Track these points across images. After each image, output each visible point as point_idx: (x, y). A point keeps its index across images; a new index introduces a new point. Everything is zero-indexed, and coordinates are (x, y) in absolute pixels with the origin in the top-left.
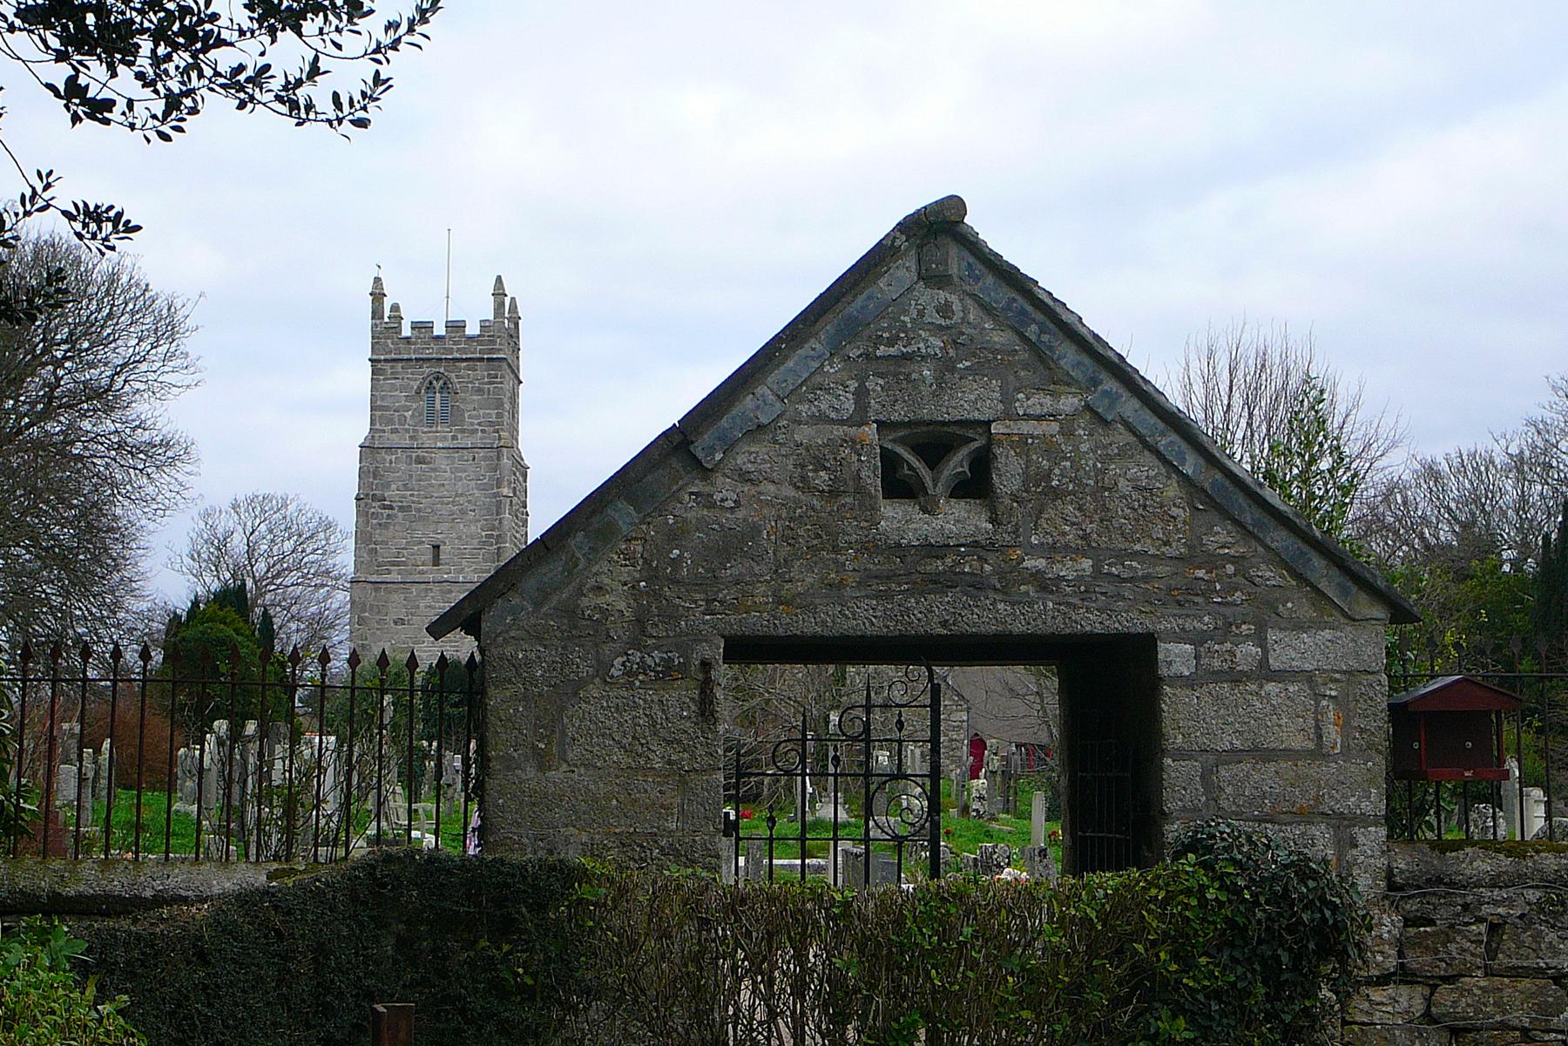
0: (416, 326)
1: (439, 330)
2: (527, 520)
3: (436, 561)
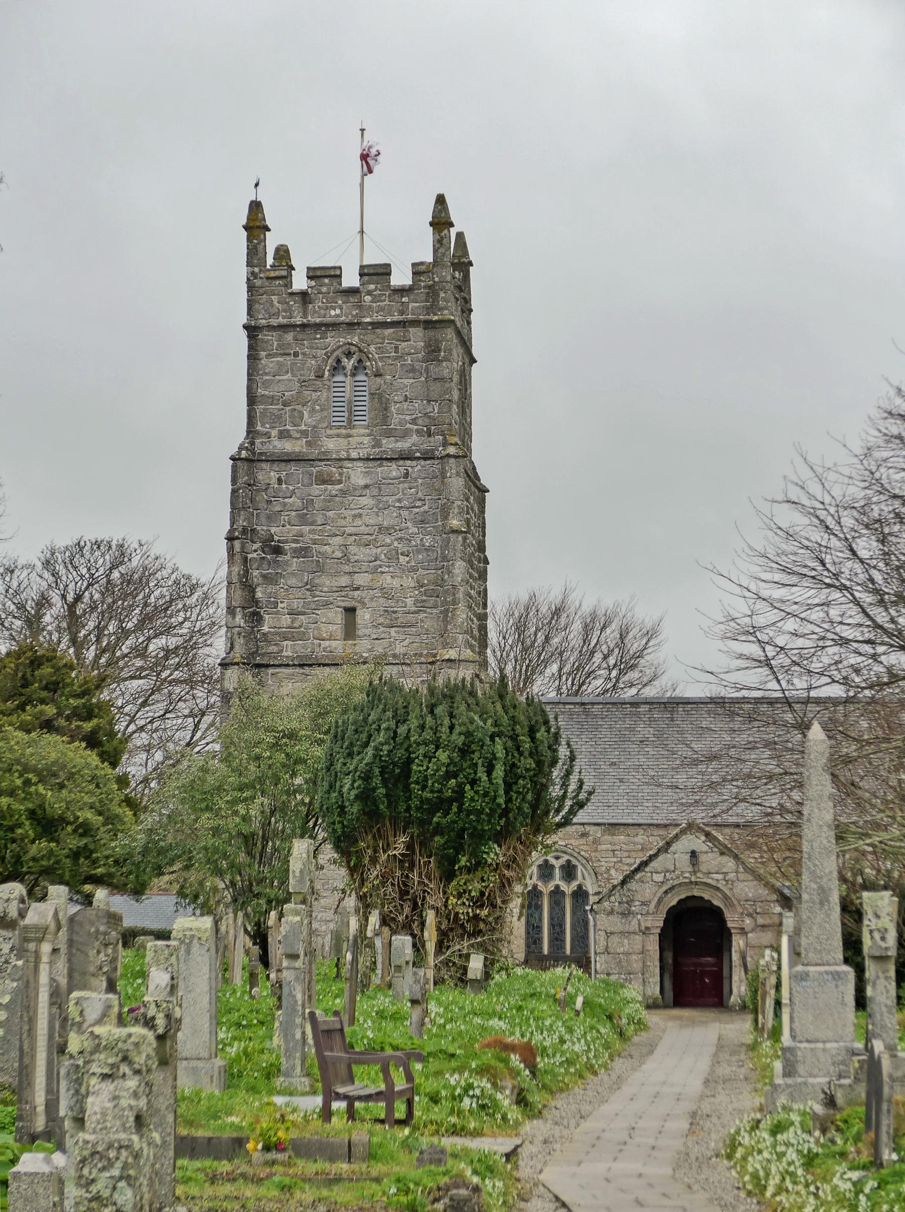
0: (314, 274)
1: (351, 279)
2: (485, 570)
3: (350, 631)
